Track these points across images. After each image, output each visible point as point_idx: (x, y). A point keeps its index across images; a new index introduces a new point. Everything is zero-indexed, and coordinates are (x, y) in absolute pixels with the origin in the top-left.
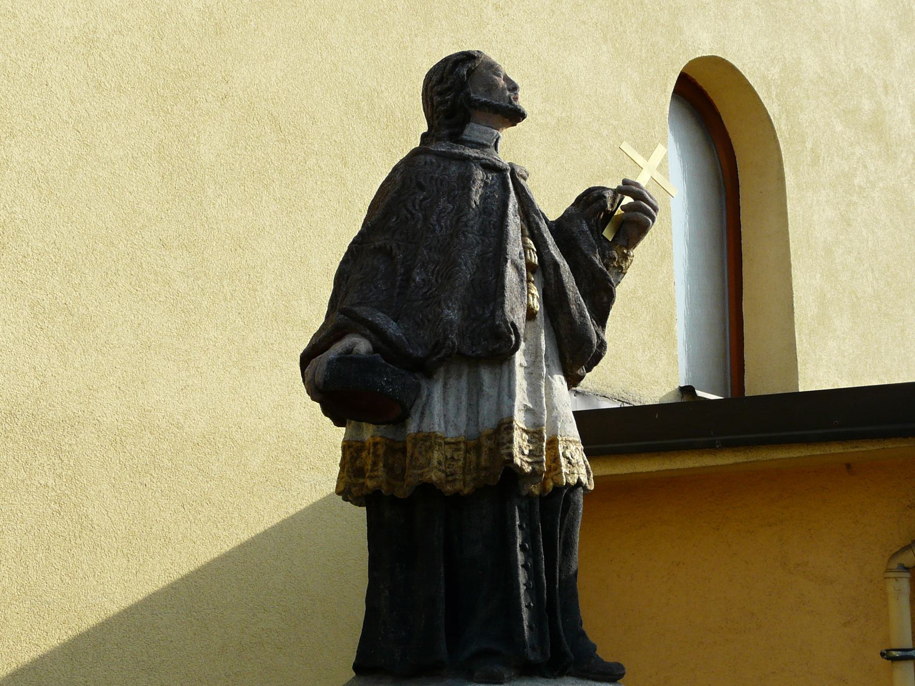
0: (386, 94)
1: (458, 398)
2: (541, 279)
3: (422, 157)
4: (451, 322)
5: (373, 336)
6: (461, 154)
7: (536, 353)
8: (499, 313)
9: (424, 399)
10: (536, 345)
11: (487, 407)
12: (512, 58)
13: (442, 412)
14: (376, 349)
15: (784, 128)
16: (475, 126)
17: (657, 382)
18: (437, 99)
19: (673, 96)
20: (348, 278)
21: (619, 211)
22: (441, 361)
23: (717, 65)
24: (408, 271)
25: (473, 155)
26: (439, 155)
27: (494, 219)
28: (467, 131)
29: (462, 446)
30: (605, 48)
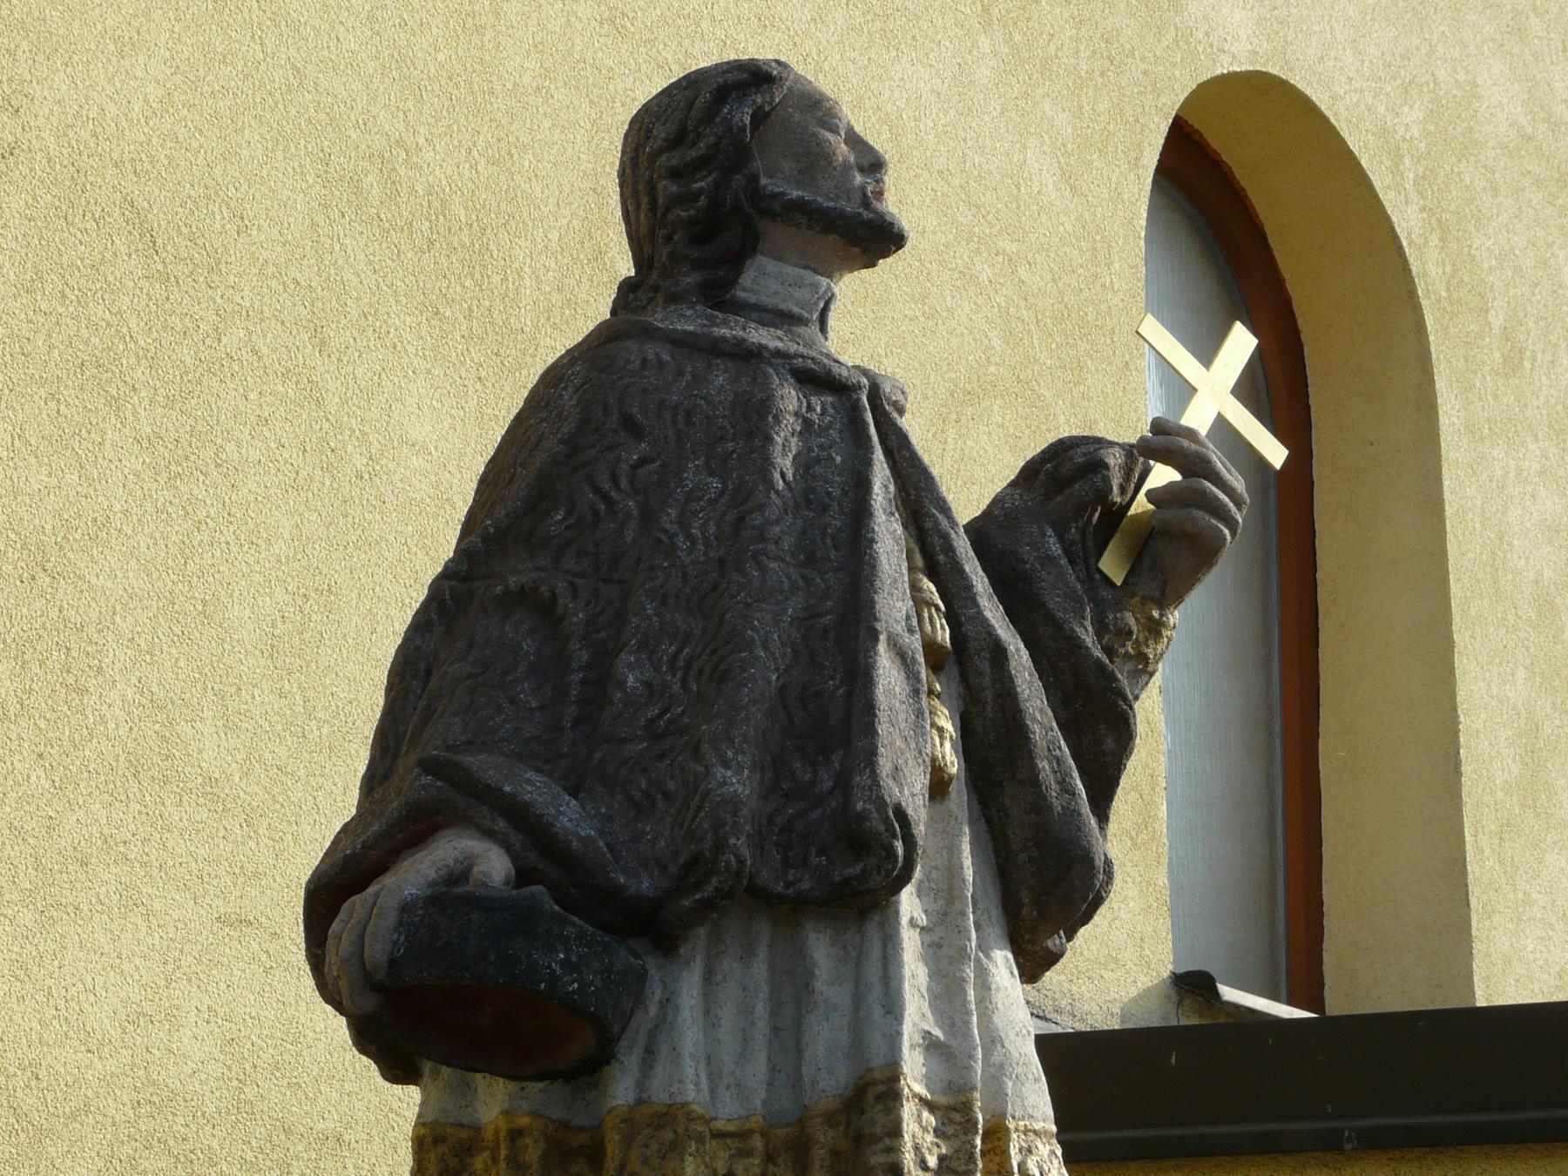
0: (428, 155)
1: (746, 1011)
2: (956, 688)
3: (632, 345)
4: (734, 803)
5: (515, 837)
6: (740, 342)
7: (951, 889)
8: (862, 779)
9: (653, 1010)
10: (949, 869)
11: (824, 1037)
12: (884, 91)
13: (702, 1043)
14: (523, 876)
15: (1433, 271)
16: (771, 265)
17: (1116, 961)
18: (667, 187)
19: (1155, 182)
20: (429, 673)
21: (1141, 505)
22: (707, 906)
23: (1264, 99)
24: (603, 657)
25: (774, 344)
26: (678, 341)
27: (835, 521)
28: (746, 279)
29: (757, 1142)
30: (985, 44)
